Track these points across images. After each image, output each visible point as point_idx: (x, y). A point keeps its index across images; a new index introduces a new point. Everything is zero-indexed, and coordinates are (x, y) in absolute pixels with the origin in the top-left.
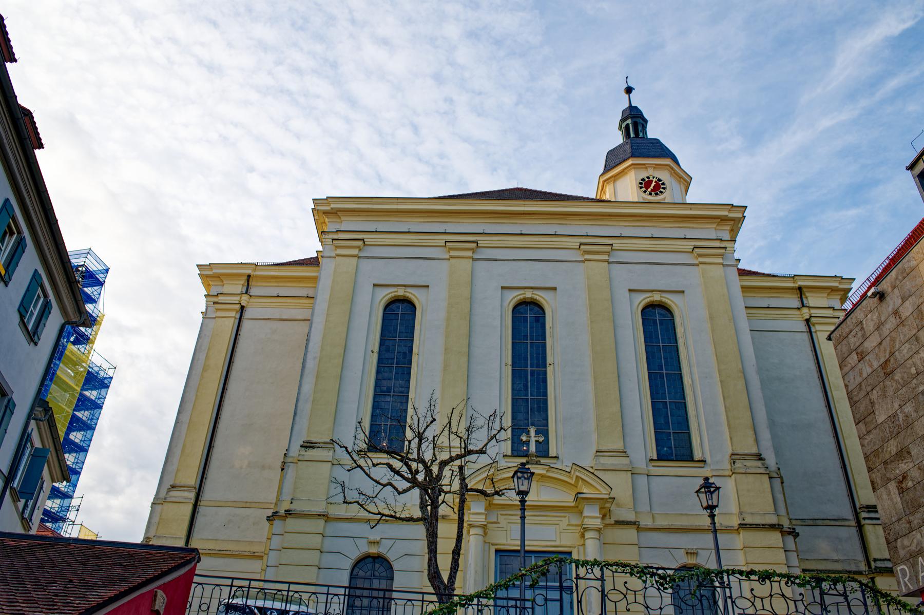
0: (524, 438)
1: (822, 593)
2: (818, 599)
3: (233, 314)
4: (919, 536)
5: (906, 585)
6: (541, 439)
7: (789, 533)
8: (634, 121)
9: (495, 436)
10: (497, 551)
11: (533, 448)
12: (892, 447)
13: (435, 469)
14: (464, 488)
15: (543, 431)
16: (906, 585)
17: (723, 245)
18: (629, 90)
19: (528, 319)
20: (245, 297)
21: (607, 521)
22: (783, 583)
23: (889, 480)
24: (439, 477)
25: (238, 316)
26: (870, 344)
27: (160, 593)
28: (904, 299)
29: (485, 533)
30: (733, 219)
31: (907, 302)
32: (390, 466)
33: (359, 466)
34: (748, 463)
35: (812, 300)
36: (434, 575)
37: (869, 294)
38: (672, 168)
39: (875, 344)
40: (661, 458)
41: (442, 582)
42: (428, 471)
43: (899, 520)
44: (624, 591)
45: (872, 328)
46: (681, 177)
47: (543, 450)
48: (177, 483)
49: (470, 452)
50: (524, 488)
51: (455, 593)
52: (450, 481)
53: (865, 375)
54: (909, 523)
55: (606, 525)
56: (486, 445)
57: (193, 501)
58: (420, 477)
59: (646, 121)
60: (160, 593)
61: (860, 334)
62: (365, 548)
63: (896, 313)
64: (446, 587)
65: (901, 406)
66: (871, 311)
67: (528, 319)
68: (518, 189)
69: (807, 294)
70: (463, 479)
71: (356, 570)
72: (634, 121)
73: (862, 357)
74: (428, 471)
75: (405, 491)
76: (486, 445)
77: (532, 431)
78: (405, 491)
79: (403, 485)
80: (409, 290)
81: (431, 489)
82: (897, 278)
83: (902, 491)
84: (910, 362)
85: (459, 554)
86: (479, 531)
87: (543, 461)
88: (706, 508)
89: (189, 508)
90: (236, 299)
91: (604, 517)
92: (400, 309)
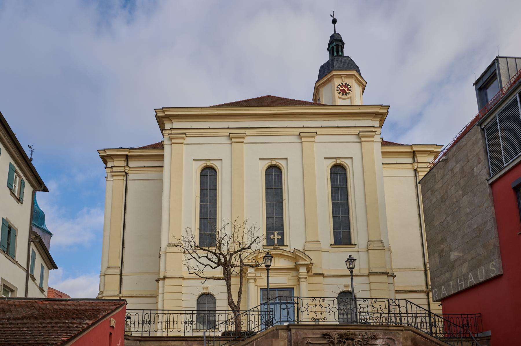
0: (272, 237)
1: (389, 305)
2: (387, 307)
3: (122, 177)
4: (444, 277)
5: (436, 297)
6: (280, 237)
7: (391, 276)
8: (336, 44)
9: (255, 240)
10: (261, 289)
11: (276, 242)
12: (439, 237)
13: (228, 257)
14: (242, 264)
15: (282, 233)
16: (436, 297)
17: (374, 130)
18: (334, 21)
19: (274, 174)
20: (127, 168)
21: (310, 273)
22: (373, 302)
23: (436, 252)
24: (230, 260)
25: (125, 179)
26: (437, 186)
27: (112, 319)
28: (457, 163)
29: (255, 281)
30: (382, 114)
31: (458, 164)
32: (207, 257)
33: (194, 257)
34: (375, 245)
35: (420, 158)
36: (230, 303)
37: (441, 160)
38: (356, 77)
39: (439, 186)
40: (336, 244)
41: (234, 304)
42: (225, 258)
43: (437, 270)
44: (307, 307)
45: (439, 178)
46: (361, 82)
47: (281, 242)
48: (110, 265)
49: (244, 249)
50: (268, 264)
51: (240, 310)
52: (235, 260)
53: (433, 202)
54: (441, 271)
55: (310, 276)
56: (251, 245)
57: (119, 273)
58: (223, 260)
59: (343, 44)
60: (112, 319)
61: (434, 181)
62: (202, 291)
63: (452, 170)
64: (236, 307)
65: (446, 218)
66: (440, 169)
67: (274, 174)
68: (269, 96)
69: (417, 155)
70: (241, 261)
71: (199, 300)
72: (336, 44)
73: (433, 192)
74: (225, 258)
75: (215, 268)
76: (251, 245)
77: (276, 233)
78: (215, 268)
79: (214, 265)
80: (212, 162)
81: (226, 265)
82: (455, 151)
83: (440, 257)
84: (454, 196)
85: (241, 293)
86: (253, 281)
87: (281, 247)
88: (349, 269)
89: (118, 277)
90: (122, 169)
91: (308, 272)
92: (209, 173)
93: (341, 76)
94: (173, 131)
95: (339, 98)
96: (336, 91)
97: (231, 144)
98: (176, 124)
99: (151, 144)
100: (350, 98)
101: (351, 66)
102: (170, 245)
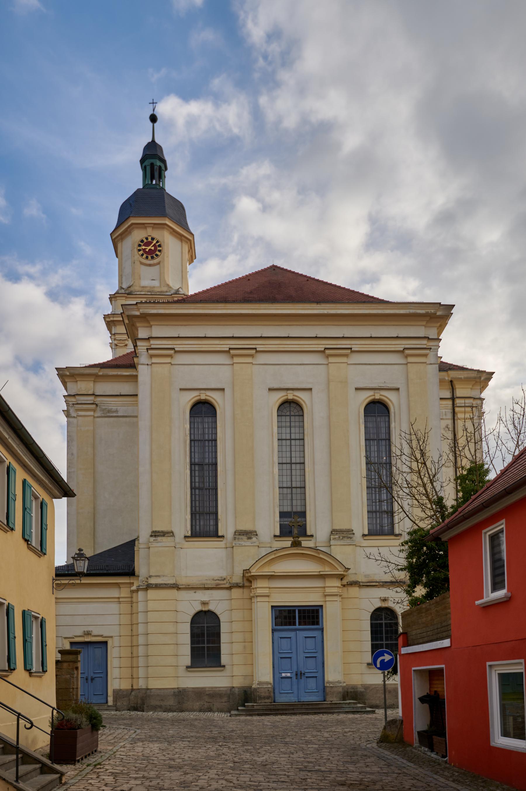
80: (209, 393)
93: (144, 226)
94: (154, 343)
95: (142, 263)
96: (136, 250)
97: (233, 364)
98: (157, 331)
99: (97, 363)
100: (159, 263)
101: (177, 212)
102: (155, 534)
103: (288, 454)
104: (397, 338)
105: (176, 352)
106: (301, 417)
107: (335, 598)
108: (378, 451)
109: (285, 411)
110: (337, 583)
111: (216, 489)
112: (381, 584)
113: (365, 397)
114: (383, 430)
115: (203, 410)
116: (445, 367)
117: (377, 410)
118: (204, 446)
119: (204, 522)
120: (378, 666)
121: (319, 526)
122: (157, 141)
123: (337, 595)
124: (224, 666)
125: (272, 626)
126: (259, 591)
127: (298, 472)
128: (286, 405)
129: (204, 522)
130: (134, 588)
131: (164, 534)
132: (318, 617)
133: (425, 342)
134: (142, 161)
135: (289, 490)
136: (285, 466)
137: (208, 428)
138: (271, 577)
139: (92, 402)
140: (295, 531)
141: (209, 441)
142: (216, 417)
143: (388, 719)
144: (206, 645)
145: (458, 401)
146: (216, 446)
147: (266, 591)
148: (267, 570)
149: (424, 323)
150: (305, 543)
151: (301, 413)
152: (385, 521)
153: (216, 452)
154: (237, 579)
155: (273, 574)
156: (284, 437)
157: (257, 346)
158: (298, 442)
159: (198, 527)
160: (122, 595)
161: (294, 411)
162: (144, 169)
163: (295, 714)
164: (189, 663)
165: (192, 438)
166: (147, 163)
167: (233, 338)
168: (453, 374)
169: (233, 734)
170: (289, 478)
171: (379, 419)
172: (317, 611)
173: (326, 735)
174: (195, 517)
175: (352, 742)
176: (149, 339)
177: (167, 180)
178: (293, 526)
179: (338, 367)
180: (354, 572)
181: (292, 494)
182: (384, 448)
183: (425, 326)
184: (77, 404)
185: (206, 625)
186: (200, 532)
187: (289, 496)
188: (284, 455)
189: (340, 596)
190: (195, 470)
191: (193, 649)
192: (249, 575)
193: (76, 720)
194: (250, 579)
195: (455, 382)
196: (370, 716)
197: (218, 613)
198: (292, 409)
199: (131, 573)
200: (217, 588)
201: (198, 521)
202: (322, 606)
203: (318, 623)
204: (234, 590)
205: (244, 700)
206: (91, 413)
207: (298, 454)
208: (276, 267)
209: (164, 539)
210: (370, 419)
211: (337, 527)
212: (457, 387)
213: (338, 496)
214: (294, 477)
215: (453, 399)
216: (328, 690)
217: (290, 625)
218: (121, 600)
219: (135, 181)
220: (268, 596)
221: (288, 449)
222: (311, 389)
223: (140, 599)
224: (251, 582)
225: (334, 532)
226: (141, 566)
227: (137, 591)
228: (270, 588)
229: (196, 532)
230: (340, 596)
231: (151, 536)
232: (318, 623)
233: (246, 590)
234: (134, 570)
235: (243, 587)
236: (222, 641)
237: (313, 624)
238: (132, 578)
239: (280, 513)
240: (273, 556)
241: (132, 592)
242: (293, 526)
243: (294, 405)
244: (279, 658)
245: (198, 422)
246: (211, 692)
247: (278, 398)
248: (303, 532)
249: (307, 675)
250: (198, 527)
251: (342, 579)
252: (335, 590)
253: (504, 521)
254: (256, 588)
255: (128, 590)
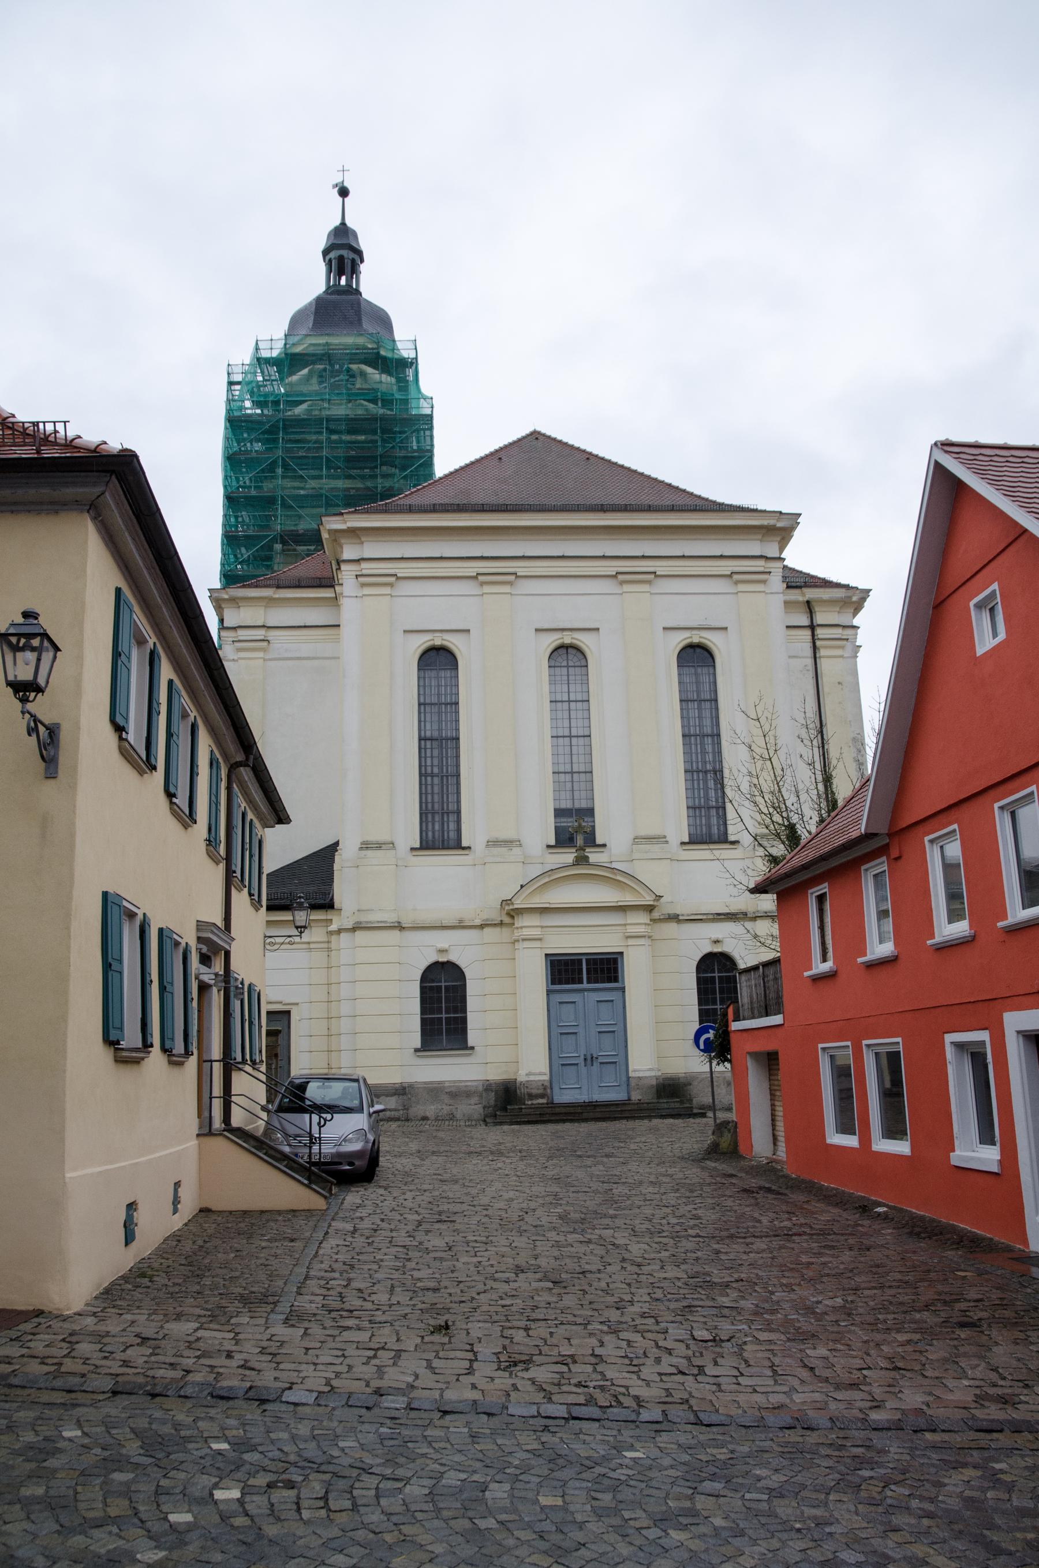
80: (446, 636)
94: (366, 567)
98: (371, 549)
102: (366, 846)
103: (566, 724)
104: (722, 557)
105: (398, 578)
106: (585, 704)
107: (641, 941)
108: (700, 717)
109: (560, 659)
110: (643, 918)
111: (458, 776)
112: (711, 917)
113: (679, 640)
114: (707, 687)
115: (437, 660)
116: (798, 581)
117: (696, 657)
118: (439, 713)
119: (440, 828)
120: (702, 1047)
121: (613, 827)
122: (349, 223)
123: (644, 937)
124: (472, 1048)
125: (547, 986)
126: (526, 932)
127: (581, 750)
128: (563, 651)
129: (440, 828)
130: (334, 927)
131: (379, 846)
132: (616, 970)
133: (762, 562)
134: (325, 253)
135: (568, 777)
136: (561, 740)
137: (446, 686)
138: (544, 911)
139: (262, 638)
140: (580, 840)
141: (446, 704)
142: (457, 669)
143: (718, 1121)
144: (444, 1016)
145: (819, 632)
146: (457, 712)
147: (536, 932)
148: (538, 901)
149: (760, 537)
150: (594, 857)
151: (583, 663)
152: (714, 821)
153: (457, 721)
154: (495, 916)
155: (547, 906)
156: (559, 698)
157: (517, 570)
158: (579, 704)
159: (430, 834)
160: (313, 940)
161: (573, 658)
162: (329, 264)
163: (586, 1120)
164: (419, 1045)
165: (422, 701)
166: (332, 255)
167: (482, 558)
168: (810, 594)
169: (502, 1147)
170: (568, 758)
171: (699, 670)
172: (615, 961)
173: (633, 1146)
174: (426, 817)
175: (669, 1154)
176: (358, 561)
177: (363, 278)
178: (575, 830)
179: (637, 598)
180: (669, 900)
181: (572, 782)
182: (708, 714)
183: (761, 541)
184: (239, 641)
185: (443, 984)
186: (433, 842)
187: (569, 785)
188: (560, 724)
189: (649, 937)
190: (425, 749)
191: (424, 1022)
192: (511, 907)
193: (718, 1064)
194: (512, 913)
195: (813, 604)
196: (698, 1120)
197: (462, 966)
198: (570, 657)
199: (328, 905)
200: (461, 926)
201: (430, 825)
202: (622, 953)
203: (616, 980)
204: (486, 930)
205: (508, 1103)
206: (261, 654)
207: (582, 758)
208: (539, 433)
209: (379, 853)
210: (686, 670)
211: (643, 833)
212: (817, 609)
213: (640, 793)
214: (575, 757)
215: (812, 627)
216: (633, 1083)
217: (574, 982)
218: (312, 946)
219: (313, 281)
220: (540, 939)
221: (566, 715)
222: (598, 629)
223: (342, 945)
224: (513, 917)
225: (638, 840)
226: (342, 891)
227: (339, 932)
228: (542, 927)
229: (427, 842)
230: (649, 937)
231: (361, 849)
232: (616, 980)
233: (505, 930)
234: (332, 899)
235: (501, 924)
236: (468, 1009)
237: (609, 981)
238: (330, 911)
239: (555, 810)
240: (547, 880)
241: (331, 933)
242: (575, 830)
243: (574, 651)
244: (558, 1034)
245: (430, 678)
246: (453, 1089)
247: (551, 641)
248: (591, 840)
249: (601, 1060)
250: (430, 834)
251: (651, 911)
252: (641, 930)
253: (826, 884)
254: (522, 928)
255: (324, 930)
